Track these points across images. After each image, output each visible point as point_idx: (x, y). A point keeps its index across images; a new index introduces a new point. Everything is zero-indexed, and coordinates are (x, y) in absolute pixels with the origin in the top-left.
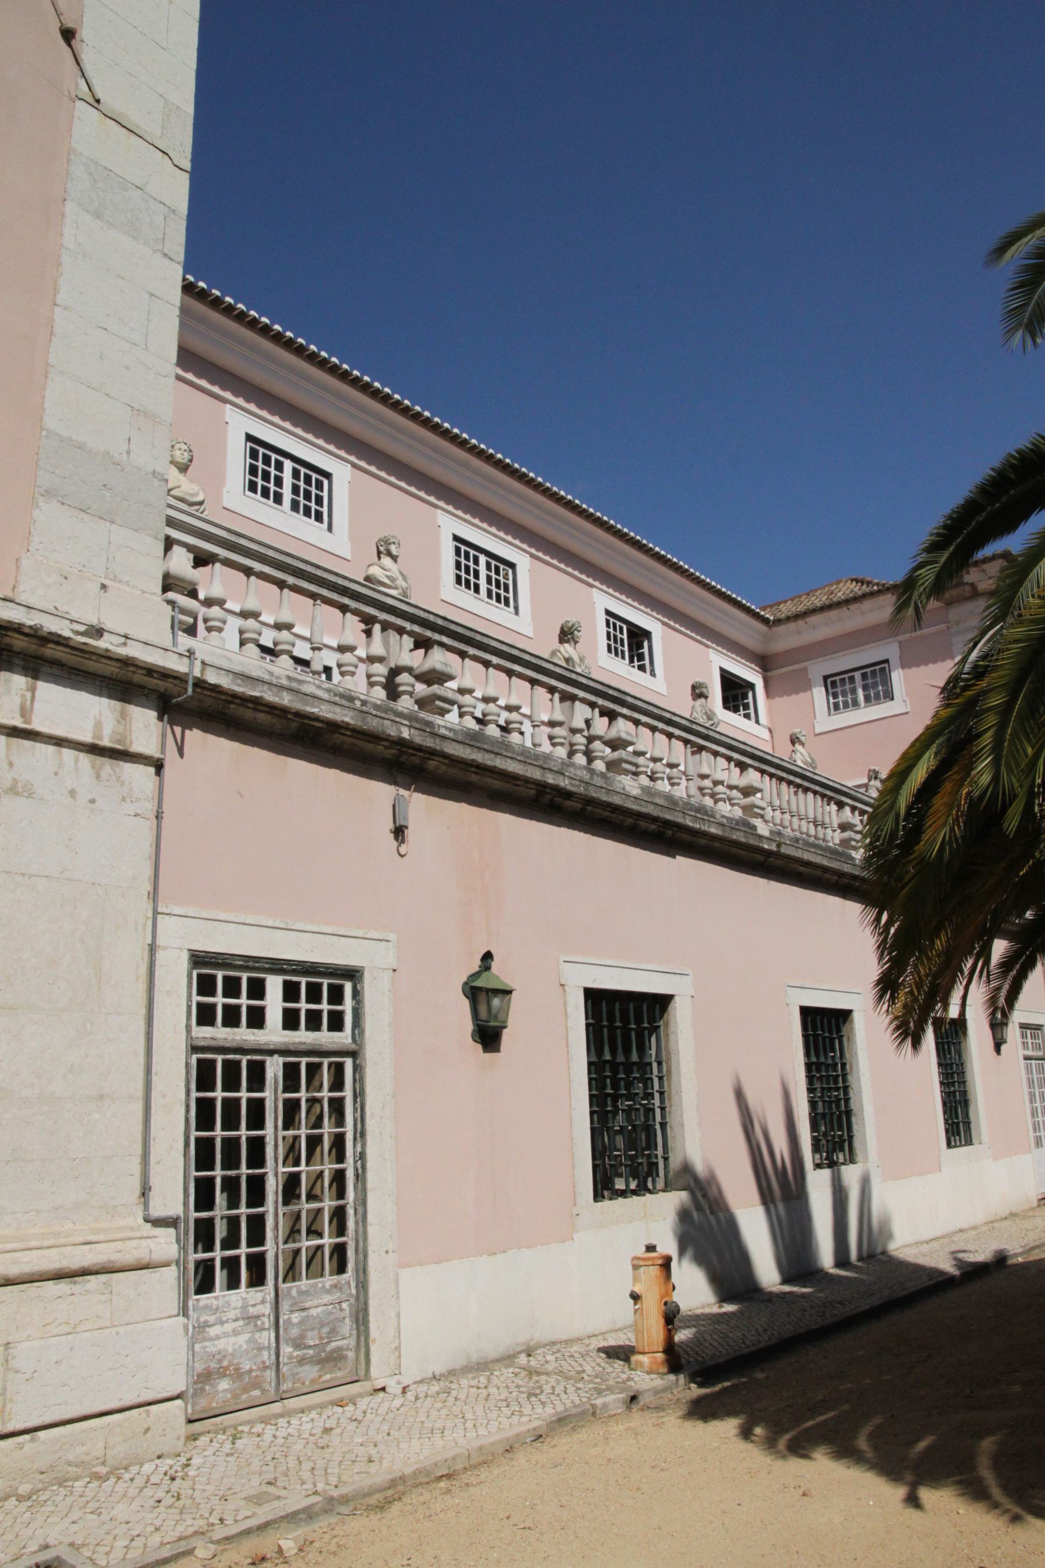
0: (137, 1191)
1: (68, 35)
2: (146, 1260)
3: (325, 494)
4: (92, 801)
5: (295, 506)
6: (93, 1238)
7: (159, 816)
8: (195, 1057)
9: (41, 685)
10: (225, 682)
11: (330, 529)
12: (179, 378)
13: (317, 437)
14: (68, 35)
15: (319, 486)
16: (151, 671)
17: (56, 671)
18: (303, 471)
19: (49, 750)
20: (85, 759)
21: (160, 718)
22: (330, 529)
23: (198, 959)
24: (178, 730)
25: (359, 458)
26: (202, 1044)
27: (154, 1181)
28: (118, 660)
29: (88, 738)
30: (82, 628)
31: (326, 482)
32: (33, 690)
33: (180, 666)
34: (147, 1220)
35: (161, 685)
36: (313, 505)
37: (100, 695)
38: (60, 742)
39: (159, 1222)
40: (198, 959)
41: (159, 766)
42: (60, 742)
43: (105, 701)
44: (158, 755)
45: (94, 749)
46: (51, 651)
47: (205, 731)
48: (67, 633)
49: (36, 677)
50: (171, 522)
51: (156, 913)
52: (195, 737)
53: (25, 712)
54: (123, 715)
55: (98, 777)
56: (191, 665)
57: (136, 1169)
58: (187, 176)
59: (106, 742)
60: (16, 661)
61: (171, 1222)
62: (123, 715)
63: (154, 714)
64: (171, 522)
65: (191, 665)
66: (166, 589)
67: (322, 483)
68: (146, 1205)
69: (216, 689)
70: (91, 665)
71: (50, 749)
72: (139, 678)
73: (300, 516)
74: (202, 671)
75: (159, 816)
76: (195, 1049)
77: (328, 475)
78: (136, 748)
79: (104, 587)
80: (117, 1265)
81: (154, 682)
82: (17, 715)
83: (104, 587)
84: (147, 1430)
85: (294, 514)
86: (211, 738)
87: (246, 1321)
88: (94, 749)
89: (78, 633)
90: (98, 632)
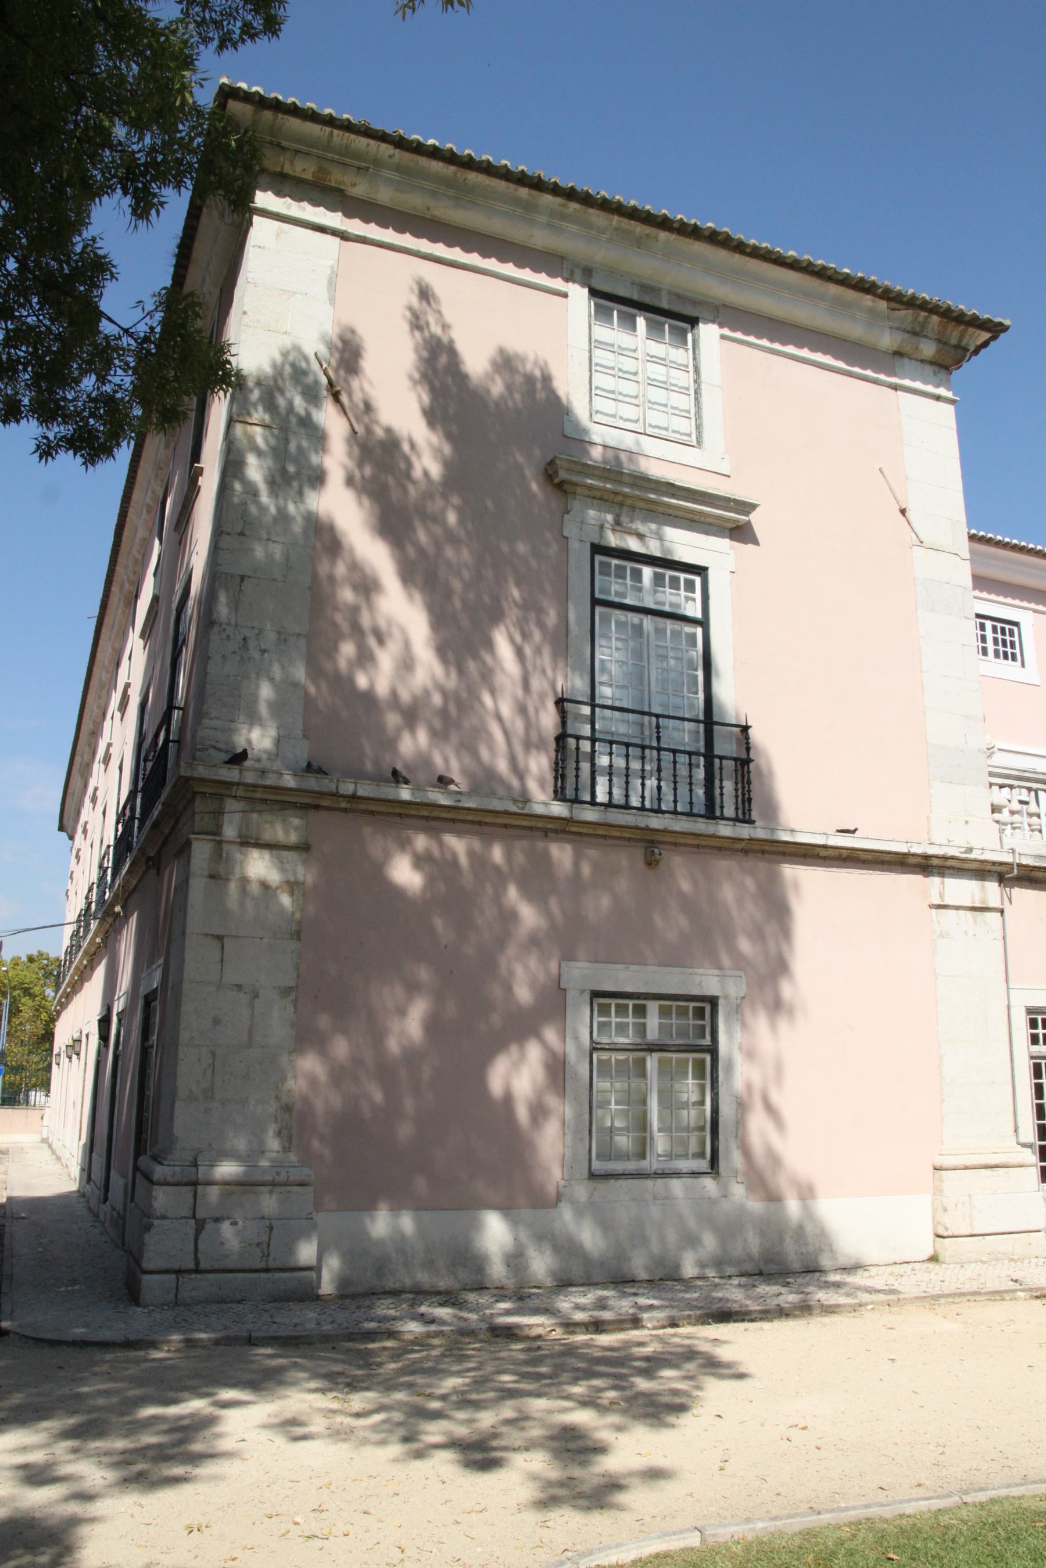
0: (1013, 1129)
1: (903, 512)
2: (1022, 1163)
3: (1016, 639)
4: (975, 935)
5: (997, 654)
6: (997, 1151)
7: (1004, 938)
8: (1032, 1061)
9: (946, 880)
10: (1031, 862)
11: (1023, 665)
12: (723, 337)
13: (1006, 596)
14: (903, 512)
15: (1012, 634)
16: (994, 863)
17: (952, 871)
18: (999, 625)
19: (953, 912)
20: (969, 914)
21: (1000, 886)
22: (1023, 665)
23: (1030, 1011)
24: (1008, 889)
25: (1037, 603)
26: (1035, 1055)
27: (1020, 1125)
28: (979, 861)
29: (970, 904)
30: (963, 850)
31: (1015, 629)
32: (943, 883)
33: (1007, 858)
34: (1018, 1144)
35: (999, 869)
36: (1009, 650)
37: (971, 880)
38: (957, 908)
39: (1024, 1145)
40: (1030, 1011)
41: (1002, 912)
42: (957, 908)
43: (974, 882)
44: (1001, 907)
45: (974, 909)
46: (949, 863)
47: (1021, 887)
48: (957, 854)
49: (943, 877)
50: (991, 774)
51: (1008, 988)
52: (1016, 892)
53: (941, 896)
54: (983, 888)
55: (976, 922)
56: (1014, 857)
57: (1012, 1118)
58: (968, 562)
59: (977, 905)
60: (935, 870)
61: (1030, 1146)
62: (983, 888)
63: (996, 884)
64: (991, 774)
65: (1014, 857)
66: (993, 812)
67: (1013, 630)
68: (1017, 1136)
69: (1026, 866)
70: (967, 866)
71: (954, 912)
72: (989, 867)
73: (1002, 660)
74: (1019, 859)
75: (1004, 938)
76: (1032, 1058)
77: (1016, 624)
78: (991, 905)
79: (967, 822)
80: (1010, 1164)
81: (994, 868)
82: (938, 898)
83: (967, 822)
84: (1030, 1244)
85: (997, 660)
86: (1024, 891)
87: (500, 1394)
88: (974, 909)
89: (962, 853)
90: (970, 850)
